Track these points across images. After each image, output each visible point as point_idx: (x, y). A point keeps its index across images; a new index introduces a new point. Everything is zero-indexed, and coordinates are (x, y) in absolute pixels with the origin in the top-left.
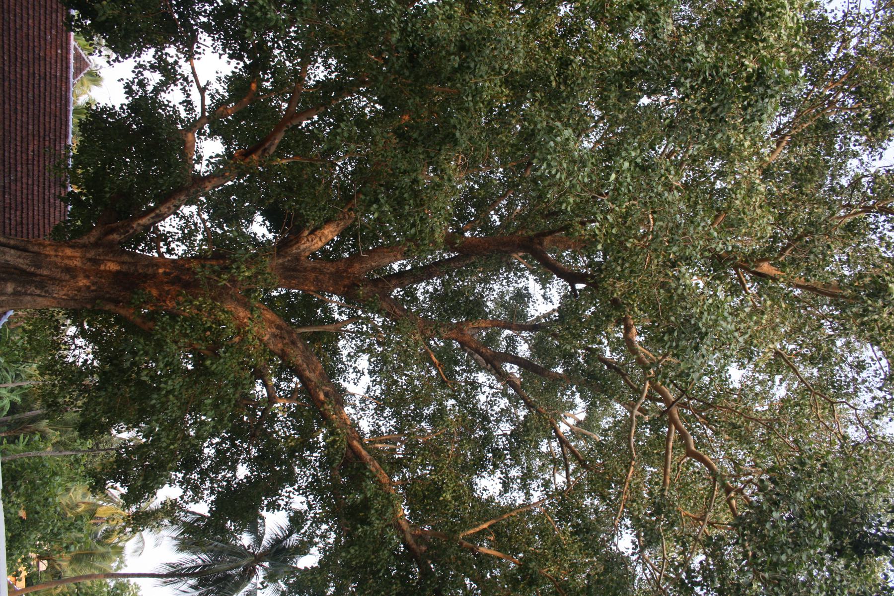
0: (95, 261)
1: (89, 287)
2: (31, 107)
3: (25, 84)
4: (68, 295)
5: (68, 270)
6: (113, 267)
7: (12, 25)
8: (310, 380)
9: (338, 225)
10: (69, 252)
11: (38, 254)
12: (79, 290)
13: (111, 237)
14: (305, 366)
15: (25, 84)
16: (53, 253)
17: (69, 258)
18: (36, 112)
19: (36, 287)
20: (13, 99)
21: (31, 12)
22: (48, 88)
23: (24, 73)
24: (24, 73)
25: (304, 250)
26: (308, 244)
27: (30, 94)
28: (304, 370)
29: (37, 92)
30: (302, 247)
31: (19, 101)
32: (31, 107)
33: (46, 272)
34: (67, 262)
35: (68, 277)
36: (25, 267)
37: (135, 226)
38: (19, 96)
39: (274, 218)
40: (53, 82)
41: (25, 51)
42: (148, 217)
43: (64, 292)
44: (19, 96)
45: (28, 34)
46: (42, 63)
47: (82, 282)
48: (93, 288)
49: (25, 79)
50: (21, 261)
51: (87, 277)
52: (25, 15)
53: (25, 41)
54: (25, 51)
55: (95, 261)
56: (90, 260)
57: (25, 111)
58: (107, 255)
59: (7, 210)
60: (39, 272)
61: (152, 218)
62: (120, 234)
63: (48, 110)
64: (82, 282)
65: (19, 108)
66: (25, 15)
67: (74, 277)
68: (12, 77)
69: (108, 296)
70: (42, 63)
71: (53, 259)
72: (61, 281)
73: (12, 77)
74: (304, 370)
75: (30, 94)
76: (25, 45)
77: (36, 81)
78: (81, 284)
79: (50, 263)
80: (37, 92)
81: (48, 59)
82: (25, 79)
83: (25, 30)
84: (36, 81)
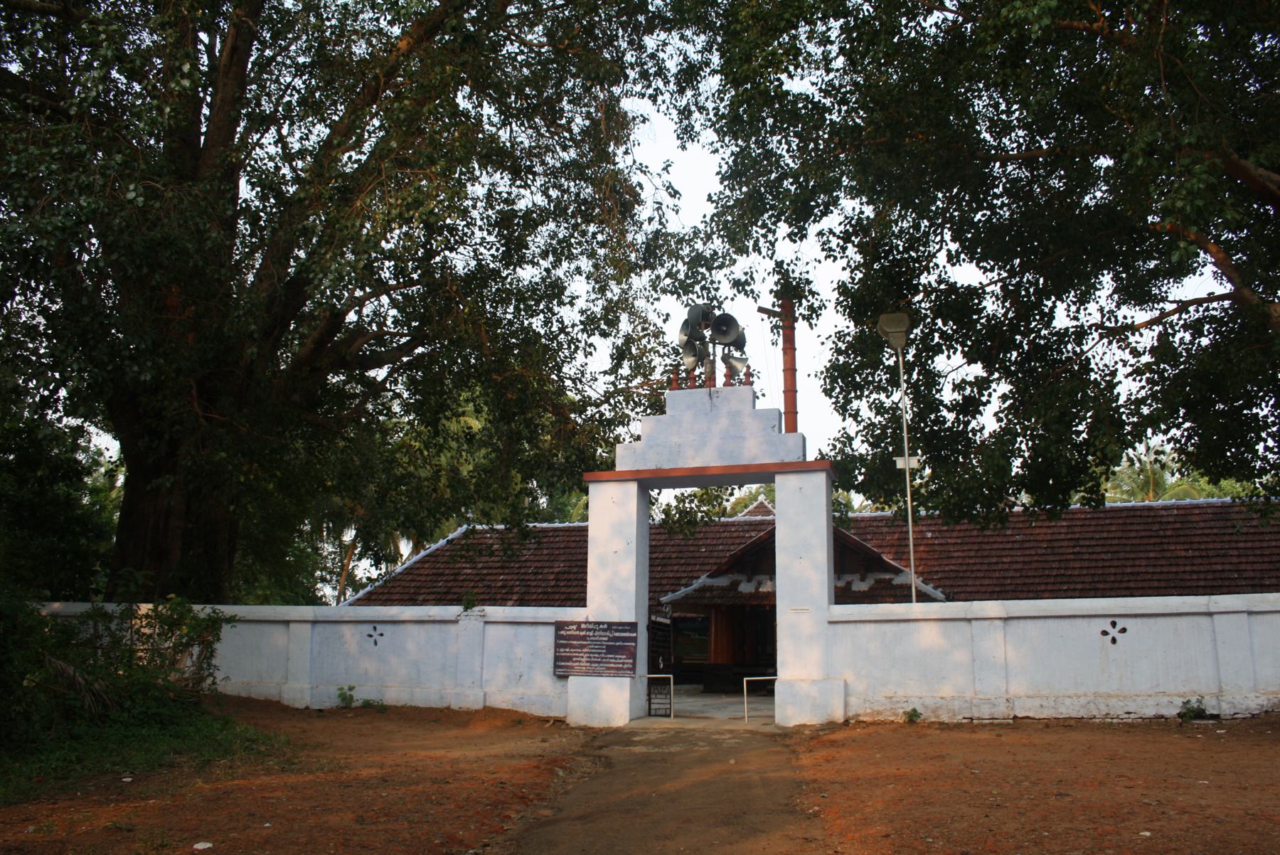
2: (1122, 555)
21: (994, 560)
27: (1103, 556)
38: (1113, 571)
40: (1077, 529)
46: (1056, 544)
52: (1000, 566)
66: (1000, 566)
68: (1089, 579)
76: (1039, 565)
80: (1099, 549)
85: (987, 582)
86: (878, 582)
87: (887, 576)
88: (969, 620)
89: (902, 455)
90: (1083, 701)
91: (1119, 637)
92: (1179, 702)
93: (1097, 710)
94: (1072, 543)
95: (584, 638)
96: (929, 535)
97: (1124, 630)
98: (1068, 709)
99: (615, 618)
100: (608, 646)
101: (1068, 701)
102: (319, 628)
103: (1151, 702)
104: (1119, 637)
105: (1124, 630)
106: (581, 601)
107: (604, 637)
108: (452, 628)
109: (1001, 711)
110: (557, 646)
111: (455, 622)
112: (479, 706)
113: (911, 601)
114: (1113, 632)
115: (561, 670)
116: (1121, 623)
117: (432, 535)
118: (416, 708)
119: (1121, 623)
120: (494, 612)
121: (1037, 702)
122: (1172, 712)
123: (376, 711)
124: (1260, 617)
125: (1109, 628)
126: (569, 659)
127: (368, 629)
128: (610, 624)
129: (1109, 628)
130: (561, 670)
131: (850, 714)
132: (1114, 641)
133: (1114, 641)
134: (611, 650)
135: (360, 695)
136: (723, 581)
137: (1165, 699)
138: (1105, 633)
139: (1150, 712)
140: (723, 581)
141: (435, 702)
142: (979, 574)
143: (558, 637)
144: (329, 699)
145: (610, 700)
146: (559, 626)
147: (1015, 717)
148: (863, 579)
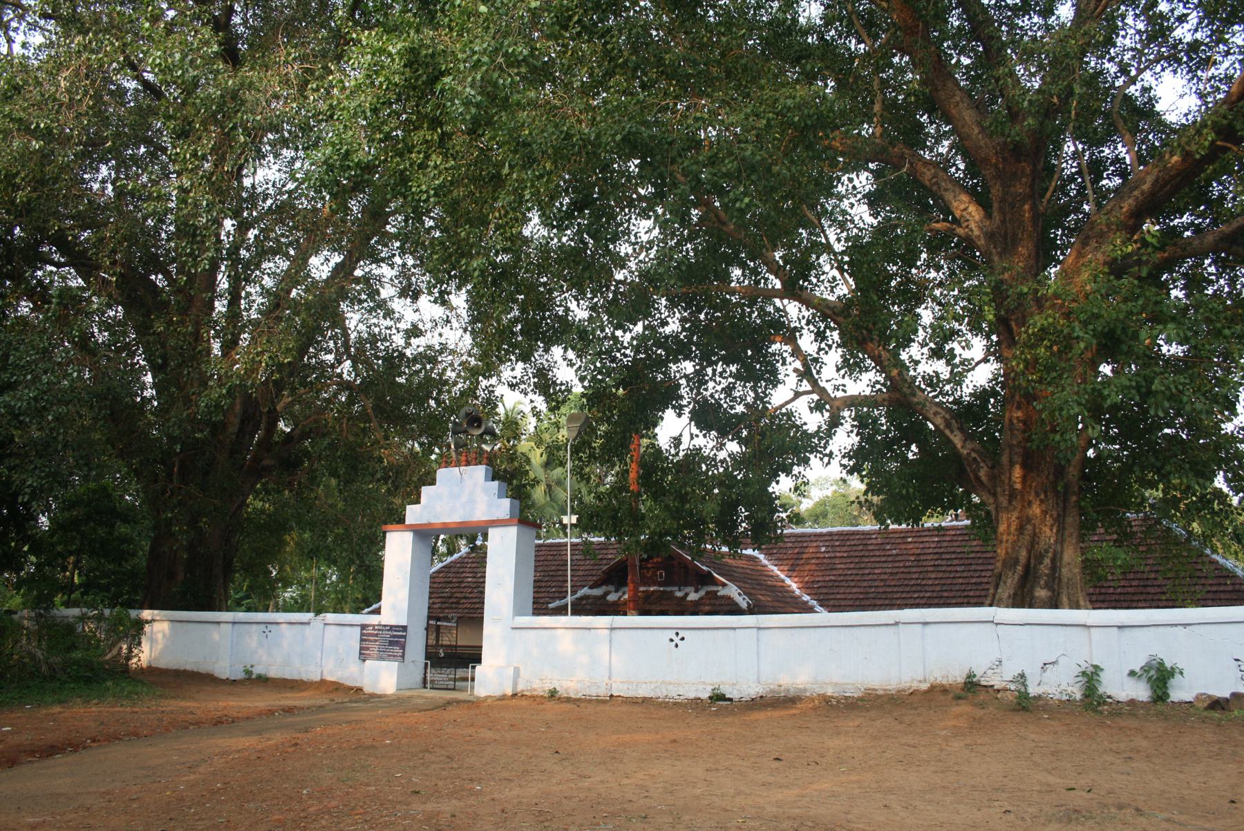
0: (1012, 495)
1: (1041, 501)
2: (973, 567)
3: (947, 575)
4: (1052, 526)
5: (1021, 529)
6: (1017, 472)
7: (881, 590)
8: (1156, 181)
9: (946, 190)
10: (1002, 528)
11: (1004, 563)
12: (1044, 512)
13: (984, 479)
14: (1136, 193)
15: (947, 575)
16: (1004, 545)
17: (1009, 526)
18: (980, 561)
19: (1041, 563)
20: (963, 587)
21: (867, 571)
22: (952, 550)
23: (933, 576)
24: (933, 576)
25: (980, 229)
26: (973, 225)
27: (959, 569)
28: (1143, 193)
29: (956, 562)
30: (976, 232)
31: (965, 581)
32: (973, 567)
33: (1023, 554)
34: (1013, 528)
35: (1029, 527)
36: (1016, 577)
37: (965, 452)
38: (961, 581)
39: (689, 235)
40: (945, 544)
41: (908, 576)
42: (952, 437)
43: (1048, 530)
44: (961, 581)
45: (891, 574)
46: (922, 558)
47: (1036, 510)
48: (1042, 496)
49: (941, 575)
50: (1009, 581)
51: (1030, 503)
52: (870, 577)
53: (898, 576)
54: (908, 576)
55: (1012, 495)
56: (1010, 502)
57: (977, 574)
58: (1002, 481)
59: (1103, 591)
60: (1023, 560)
61: (952, 432)
62: (979, 468)
63: (978, 549)
64: (1036, 510)
65: (974, 580)
66: (870, 577)
67: (1029, 520)
68: (938, 588)
69: (1051, 477)
70: (922, 558)
71: (1009, 545)
72: (1035, 534)
73: (938, 588)
74: (1143, 193)
75: (959, 569)
76: (903, 576)
77: (944, 563)
78: (1038, 511)
79: (1013, 548)
80: (956, 562)
81: (918, 551)
82: (941, 575)
83: (886, 577)
84: (944, 563)
85: (855, 590)
86: (708, 593)
87: (715, 588)
88: (734, 629)
89: (566, 514)
90: (653, 686)
91: (680, 643)
92: (710, 688)
93: (660, 693)
94: (935, 557)
95: (376, 635)
96: (823, 549)
97: (683, 639)
98: (643, 692)
99: (393, 622)
100: (392, 641)
101: (644, 686)
102: (237, 626)
103: (693, 688)
104: (680, 643)
105: (683, 639)
106: (377, 612)
107: (387, 634)
108: (306, 627)
109: (603, 692)
110: (362, 640)
111: (308, 623)
112: (318, 678)
113: (566, 614)
114: (677, 640)
115: (363, 657)
116: (682, 634)
117: (256, 569)
118: (285, 680)
119: (682, 634)
120: (330, 617)
121: (626, 686)
122: (705, 695)
123: (263, 681)
124: (766, 632)
125: (674, 637)
126: (368, 649)
127: (263, 627)
128: (392, 627)
129: (674, 637)
130: (363, 657)
131: (520, 688)
132: (677, 646)
133: (677, 646)
134: (391, 643)
135: (257, 671)
136: (597, 592)
137: (701, 687)
138: (672, 640)
139: (692, 695)
140: (597, 592)
141: (296, 677)
142: (852, 584)
143: (362, 634)
144: (240, 675)
145: (384, 677)
146: (363, 627)
147: (611, 696)
148: (696, 591)
